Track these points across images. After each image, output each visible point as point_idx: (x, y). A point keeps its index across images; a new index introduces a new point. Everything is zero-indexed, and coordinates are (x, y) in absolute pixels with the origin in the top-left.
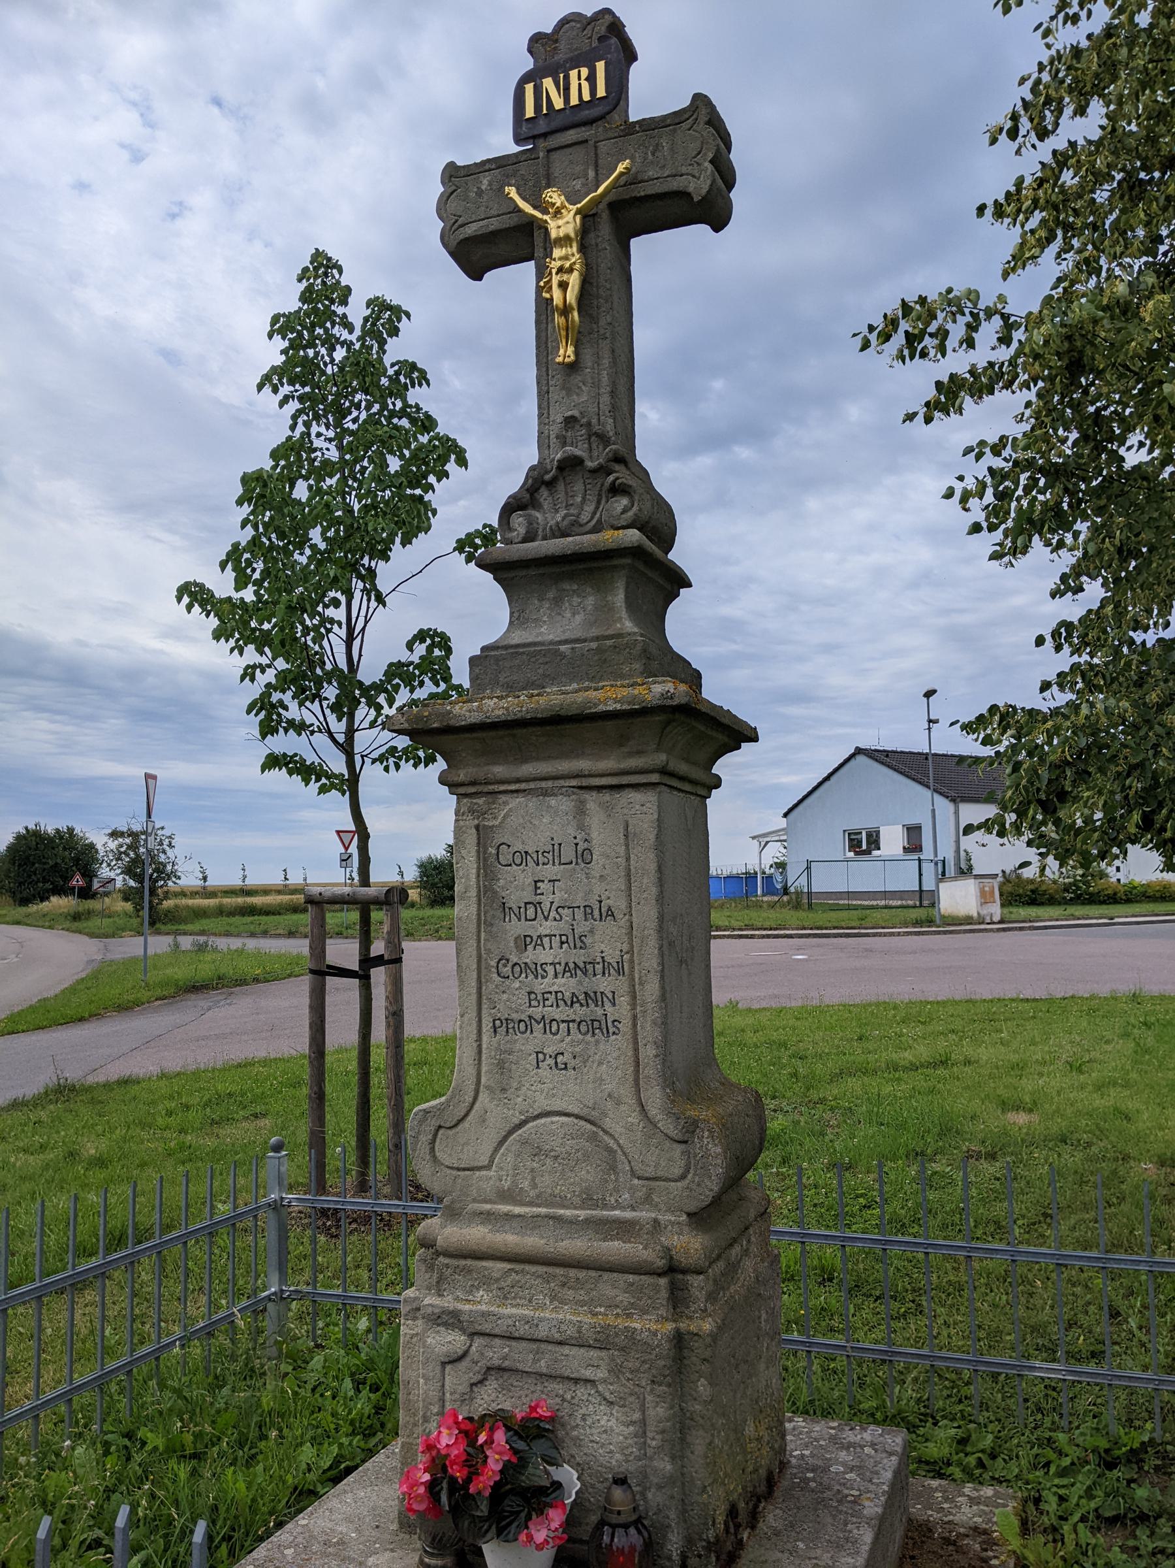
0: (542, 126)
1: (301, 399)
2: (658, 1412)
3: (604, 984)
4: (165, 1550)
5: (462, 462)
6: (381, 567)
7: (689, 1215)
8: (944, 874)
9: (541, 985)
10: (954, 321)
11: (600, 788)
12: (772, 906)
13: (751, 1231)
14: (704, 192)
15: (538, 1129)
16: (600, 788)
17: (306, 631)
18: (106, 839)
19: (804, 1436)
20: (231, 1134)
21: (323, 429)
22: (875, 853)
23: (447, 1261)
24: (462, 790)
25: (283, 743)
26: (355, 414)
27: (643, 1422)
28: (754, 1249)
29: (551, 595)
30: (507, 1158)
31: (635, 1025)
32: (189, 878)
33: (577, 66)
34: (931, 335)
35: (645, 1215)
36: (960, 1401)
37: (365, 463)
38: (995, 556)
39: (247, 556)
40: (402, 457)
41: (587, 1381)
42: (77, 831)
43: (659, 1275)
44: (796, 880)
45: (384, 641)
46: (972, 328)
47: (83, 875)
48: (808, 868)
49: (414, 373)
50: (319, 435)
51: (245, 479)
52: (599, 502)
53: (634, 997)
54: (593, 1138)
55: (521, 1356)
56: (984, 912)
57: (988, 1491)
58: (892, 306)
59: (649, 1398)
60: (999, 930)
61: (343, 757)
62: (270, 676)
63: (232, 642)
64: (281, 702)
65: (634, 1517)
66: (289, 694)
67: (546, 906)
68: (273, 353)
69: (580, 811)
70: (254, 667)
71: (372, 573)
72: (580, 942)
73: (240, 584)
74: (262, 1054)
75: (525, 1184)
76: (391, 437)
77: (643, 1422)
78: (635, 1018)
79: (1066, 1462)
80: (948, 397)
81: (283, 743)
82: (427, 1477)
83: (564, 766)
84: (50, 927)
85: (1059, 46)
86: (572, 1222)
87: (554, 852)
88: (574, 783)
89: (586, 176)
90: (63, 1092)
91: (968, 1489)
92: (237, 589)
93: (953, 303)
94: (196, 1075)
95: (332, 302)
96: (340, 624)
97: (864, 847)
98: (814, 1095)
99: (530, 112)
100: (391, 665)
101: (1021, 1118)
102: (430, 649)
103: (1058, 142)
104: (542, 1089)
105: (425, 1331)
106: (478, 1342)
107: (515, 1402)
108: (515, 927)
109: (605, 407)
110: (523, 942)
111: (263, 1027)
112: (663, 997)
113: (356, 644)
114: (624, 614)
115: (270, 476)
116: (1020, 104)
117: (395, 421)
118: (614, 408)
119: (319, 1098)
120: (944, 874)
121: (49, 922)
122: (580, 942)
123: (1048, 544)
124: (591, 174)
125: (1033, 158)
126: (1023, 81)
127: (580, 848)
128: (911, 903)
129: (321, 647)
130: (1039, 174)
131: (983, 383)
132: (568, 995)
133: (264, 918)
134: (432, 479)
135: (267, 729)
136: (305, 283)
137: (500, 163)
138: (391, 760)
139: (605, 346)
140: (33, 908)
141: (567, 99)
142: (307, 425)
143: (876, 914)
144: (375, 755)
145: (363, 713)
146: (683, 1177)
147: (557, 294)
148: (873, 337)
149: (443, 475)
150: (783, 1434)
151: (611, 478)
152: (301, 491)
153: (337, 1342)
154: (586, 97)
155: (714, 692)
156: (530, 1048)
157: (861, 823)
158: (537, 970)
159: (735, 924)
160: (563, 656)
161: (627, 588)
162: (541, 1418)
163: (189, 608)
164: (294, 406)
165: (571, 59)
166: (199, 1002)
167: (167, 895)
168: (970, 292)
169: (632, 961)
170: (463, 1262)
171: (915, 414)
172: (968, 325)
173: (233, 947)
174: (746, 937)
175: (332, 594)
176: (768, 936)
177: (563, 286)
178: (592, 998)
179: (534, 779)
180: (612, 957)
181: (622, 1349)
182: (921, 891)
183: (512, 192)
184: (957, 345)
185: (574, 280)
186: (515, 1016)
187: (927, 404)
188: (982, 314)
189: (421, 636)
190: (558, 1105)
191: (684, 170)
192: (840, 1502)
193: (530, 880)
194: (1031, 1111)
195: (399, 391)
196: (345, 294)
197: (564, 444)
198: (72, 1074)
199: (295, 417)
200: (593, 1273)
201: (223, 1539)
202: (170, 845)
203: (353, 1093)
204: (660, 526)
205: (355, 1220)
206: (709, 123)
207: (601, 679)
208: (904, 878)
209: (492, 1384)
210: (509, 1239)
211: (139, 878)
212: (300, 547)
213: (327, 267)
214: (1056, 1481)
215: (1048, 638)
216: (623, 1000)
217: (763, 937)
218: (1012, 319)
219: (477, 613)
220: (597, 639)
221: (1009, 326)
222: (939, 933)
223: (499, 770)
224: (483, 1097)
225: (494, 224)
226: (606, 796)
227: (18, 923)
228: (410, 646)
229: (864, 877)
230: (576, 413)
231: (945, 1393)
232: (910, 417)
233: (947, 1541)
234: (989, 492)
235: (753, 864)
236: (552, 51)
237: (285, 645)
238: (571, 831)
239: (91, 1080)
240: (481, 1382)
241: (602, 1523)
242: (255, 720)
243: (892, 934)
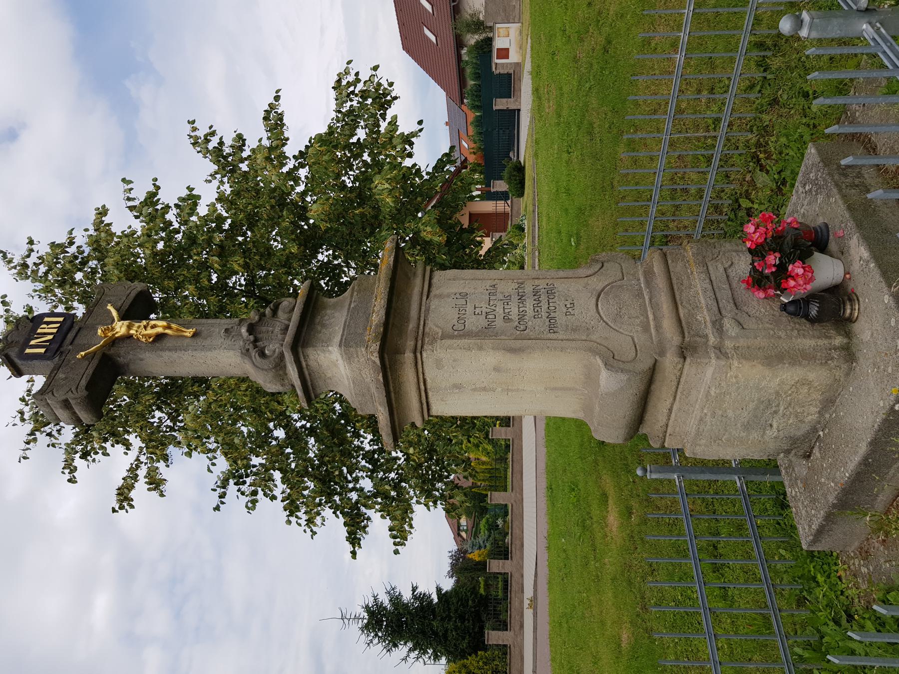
3: (528, 288)
9: (530, 311)
27: (736, 251)
29: (319, 328)
54: (607, 294)
69: (440, 296)
75: (638, 321)
87: (461, 310)
88: (424, 298)
108: (499, 323)
110: (507, 319)
156: (565, 318)
158: (522, 317)
178: (536, 293)
186: (547, 323)
216: (537, 282)
223: (412, 325)
224: (594, 337)
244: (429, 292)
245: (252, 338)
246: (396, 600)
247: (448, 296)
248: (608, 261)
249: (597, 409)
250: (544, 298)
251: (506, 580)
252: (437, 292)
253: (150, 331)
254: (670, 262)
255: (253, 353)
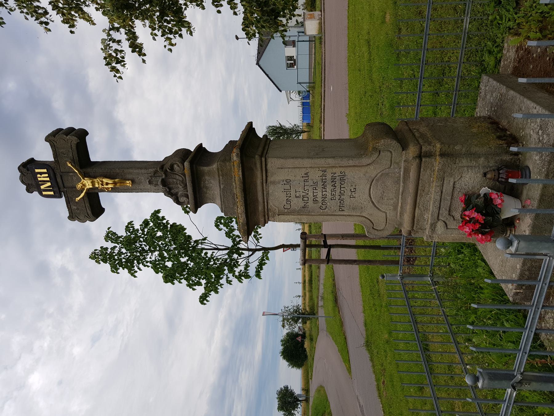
0: (56, 189)
1: (139, 263)
2: (464, 162)
3: (329, 176)
4: (504, 315)
5: (158, 211)
6: (194, 238)
7: (403, 150)
8: (303, 32)
10: (112, 47)
11: (266, 176)
12: (313, 97)
13: (411, 128)
14: (76, 138)
15: (375, 196)
16: (266, 176)
17: (215, 263)
18: (285, 329)
19: (482, 111)
20: (383, 291)
21: (149, 257)
22: (295, 58)
23: (415, 227)
24: (267, 220)
25: (252, 271)
26: (143, 246)
28: (417, 127)
29: (205, 190)
30: (383, 208)
31: (342, 167)
32: (299, 302)
33: (37, 178)
34: (117, 55)
35: (402, 165)
36: (477, 51)
37: (160, 243)
38: (191, 34)
39: (191, 282)
40: (157, 231)
41: (454, 184)
42: (282, 338)
43: (421, 161)
44: (304, 88)
45: (218, 238)
46: (114, 41)
47: (297, 337)
48: (300, 83)
49: (129, 226)
50: (150, 258)
51: (166, 282)
52: (176, 174)
53: (333, 167)
54: (377, 180)
55: (446, 204)
56: (317, 18)
57: (506, 45)
58: (108, 69)
59: (460, 165)
60: (324, 12)
61: (257, 252)
62: (230, 275)
63: (219, 287)
64: (239, 272)
65: (497, 171)
66: (235, 269)
67: (304, 194)
68: (124, 272)
69: (274, 183)
70: (227, 280)
71: (196, 242)
72: (316, 183)
73: (199, 284)
74: (358, 279)
76: (151, 235)
77: (468, 167)
78: (340, 167)
79: (498, 17)
80: (137, 48)
81: (252, 271)
82: (480, 235)
83: (259, 188)
84: (315, 348)
85: (15, 5)
86: (404, 188)
89: (72, 176)
90: (368, 344)
91: (505, 52)
92: (202, 285)
93: (106, 48)
94: (364, 301)
95: (106, 253)
96: (213, 252)
97: (293, 62)
98: (378, 90)
99: (52, 193)
100: (226, 236)
101: (388, 17)
102: (221, 223)
103: (49, 8)
104: (362, 196)
105: (437, 234)
106: (440, 218)
107: (460, 206)
108: (311, 204)
109: (146, 171)
110: (315, 201)
111: (350, 280)
112: (334, 157)
113: (220, 247)
114: (211, 167)
115: (165, 274)
116: (37, 21)
117: (145, 233)
118: (146, 168)
119: (370, 262)
120: (303, 32)
121: (313, 348)
122: (316, 183)
123: (186, 9)
124: (71, 174)
125: (55, 18)
126: (27, 19)
127: (286, 183)
128: (314, 45)
129: (220, 259)
130: (60, 15)
131: (132, 37)
132: (332, 188)
133: (313, 277)
134: (164, 221)
135: (247, 277)
136: (101, 262)
137: (68, 203)
138: (258, 237)
139: (126, 171)
140: (308, 354)
141: (48, 181)
142: (147, 262)
143: (317, 59)
144: (256, 242)
145: (242, 245)
146: (391, 152)
147: (110, 186)
148: (118, 75)
149: (163, 218)
150: (480, 117)
151: (168, 170)
152: (169, 264)
153: (448, 258)
154: (47, 175)
155: (236, 137)
157: (284, 63)
158: (324, 197)
159: (319, 112)
160: (224, 187)
161: (204, 166)
162: (465, 199)
163: (207, 301)
164: (141, 266)
165: (35, 179)
166: (341, 299)
167: (305, 309)
168: (102, 42)
169: (322, 167)
170: (415, 222)
171: (143, 59)
172: (113, 42)
173: (323, 287)
174: (324, 107)
175: (203, 254)
176: (324, 99)
177: (107, 184)
178: (333, 180)
179: (263, 197)
180: (321, 173)
181: (444, 173)
182: (309, 41)
183: (78, 199)
184: (120, 46)
185: (105, 180)
186: (339, 204)
187: (140, 55)
188: (109, 38)
189: (217, 226)
191: (69, 145)
192: (501, 100)
193: (296, 199)
194: (385, 13)
195: (135, 231)
196: (104, 249)
197: (157, 184)
198: (363, 341)
199: (145, 266)
200: (420, 182)
201: (502, 297)
202: (288, 308)
203: (372, 251)
204: (183, 154)
205: (411, 251)
206: (54, 136)
207: (232, 175)
208: (304, 47)
209: (454, 213)
210: (409, 208)
211: (299, 318)
212: (187, 265)
213: (95, 254)
214: (504, 21)
215: (218, 9)
216: (334, 170)
217: (324, 101)
218: (111, 27)
219: (211, 211)
220: (219, 176)
221: (113, 28)
222: (325, 35)
223: (260, 208)
225: (88, 205)
226: (269, 174)
227: (313, 359)
228: (220, 230)
229: (304, 62)
230: (148, 180)
231: (474, 56)
232: (144, 61)
233: (519, 62)
234: (169, 36)
235: (299, 103)
236: (32, 185)
237: (219, 272)
239: (365, 336)
240: (453, 217)
241: (498, 180)
242: (245, 280)
243: (325, 53)
250: (338, 185)
254: (422, 170)
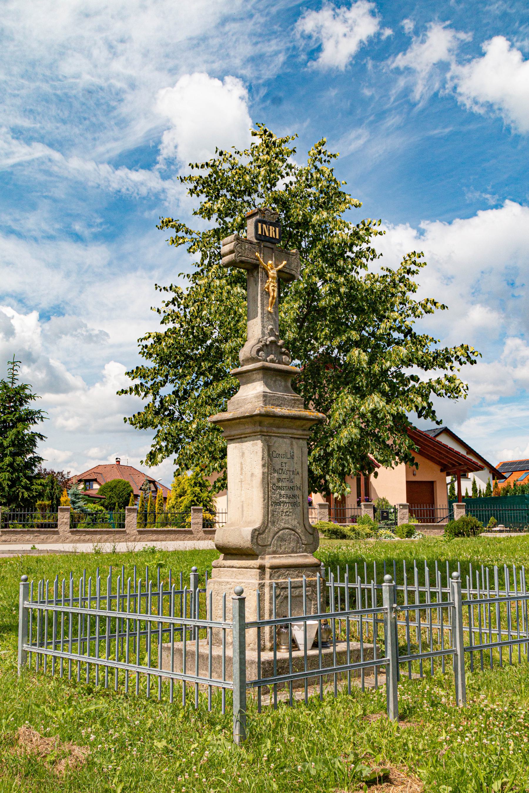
3: (297, 492)
87: (285, 455)
99: (260, 232)
178: (294, 496)
190: (287, 526)
216: (301, 497)
238: (290, 449)
244: (295, 438)
245: (268, 343)
246: (30, 417)
247: (292, 448)
248: (314, 538)
249: (232, 528)
251: (51, 526)
252: (294, 443)
253: (271, 288)
255: (260, 345)
